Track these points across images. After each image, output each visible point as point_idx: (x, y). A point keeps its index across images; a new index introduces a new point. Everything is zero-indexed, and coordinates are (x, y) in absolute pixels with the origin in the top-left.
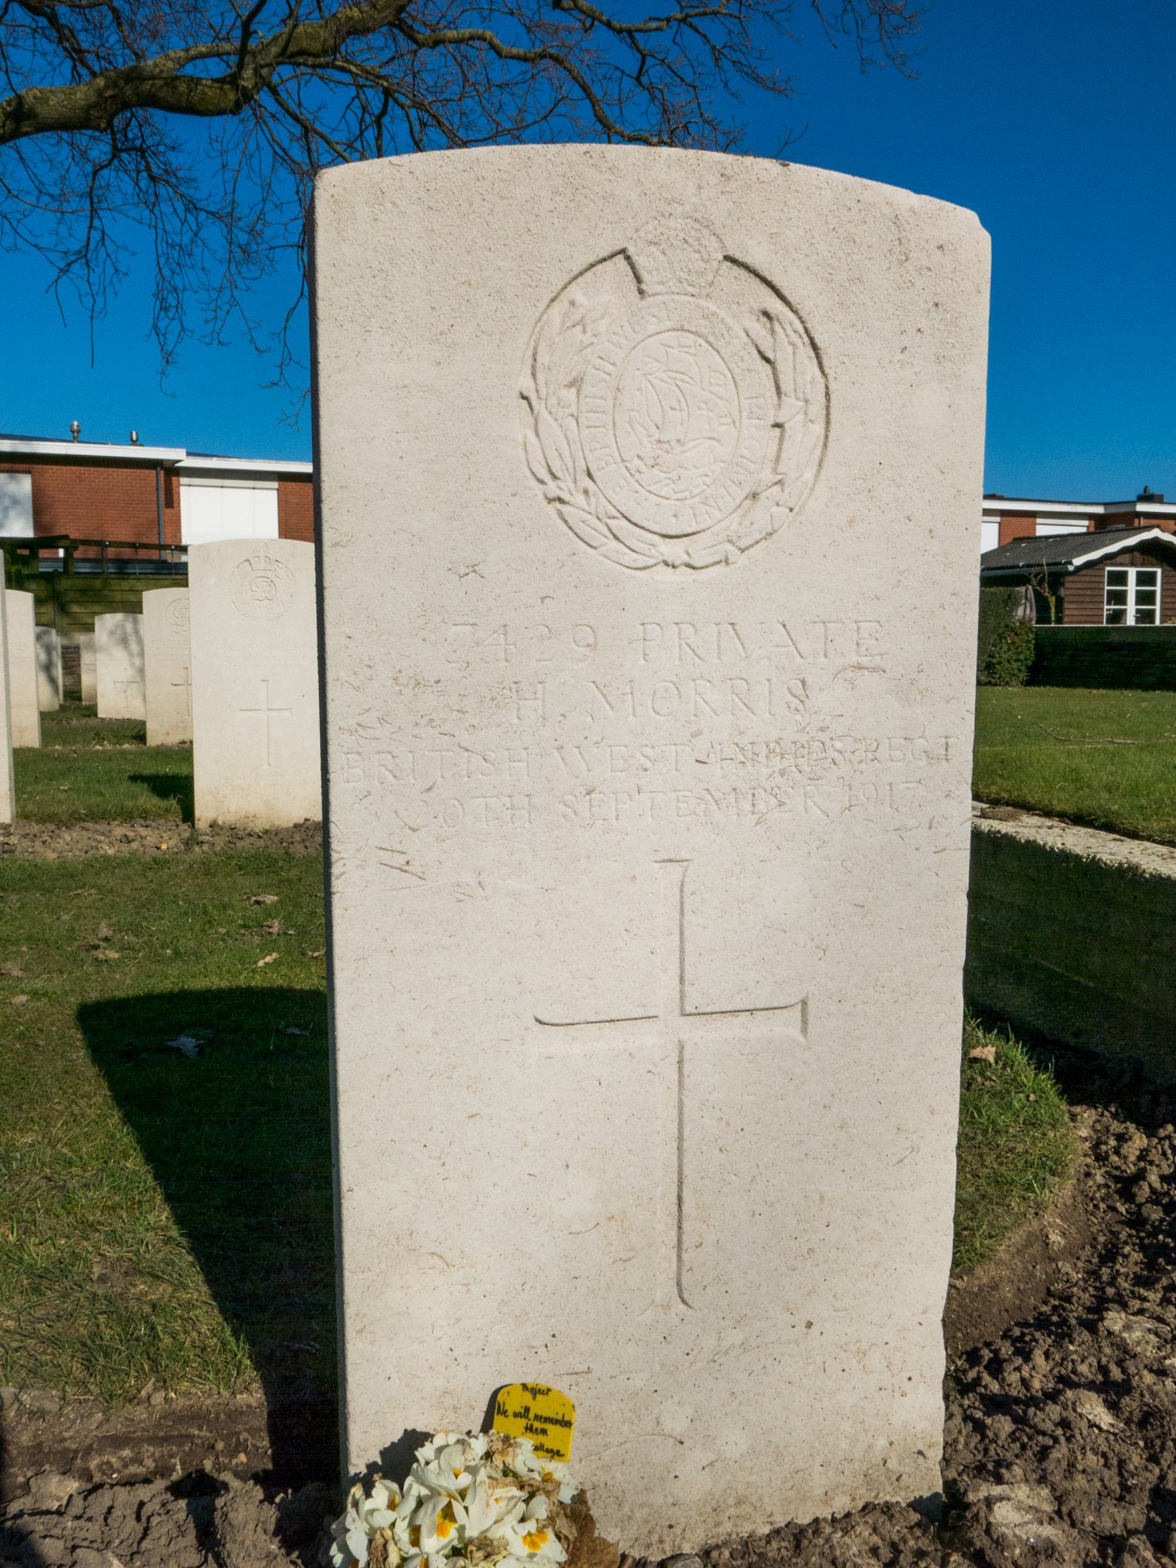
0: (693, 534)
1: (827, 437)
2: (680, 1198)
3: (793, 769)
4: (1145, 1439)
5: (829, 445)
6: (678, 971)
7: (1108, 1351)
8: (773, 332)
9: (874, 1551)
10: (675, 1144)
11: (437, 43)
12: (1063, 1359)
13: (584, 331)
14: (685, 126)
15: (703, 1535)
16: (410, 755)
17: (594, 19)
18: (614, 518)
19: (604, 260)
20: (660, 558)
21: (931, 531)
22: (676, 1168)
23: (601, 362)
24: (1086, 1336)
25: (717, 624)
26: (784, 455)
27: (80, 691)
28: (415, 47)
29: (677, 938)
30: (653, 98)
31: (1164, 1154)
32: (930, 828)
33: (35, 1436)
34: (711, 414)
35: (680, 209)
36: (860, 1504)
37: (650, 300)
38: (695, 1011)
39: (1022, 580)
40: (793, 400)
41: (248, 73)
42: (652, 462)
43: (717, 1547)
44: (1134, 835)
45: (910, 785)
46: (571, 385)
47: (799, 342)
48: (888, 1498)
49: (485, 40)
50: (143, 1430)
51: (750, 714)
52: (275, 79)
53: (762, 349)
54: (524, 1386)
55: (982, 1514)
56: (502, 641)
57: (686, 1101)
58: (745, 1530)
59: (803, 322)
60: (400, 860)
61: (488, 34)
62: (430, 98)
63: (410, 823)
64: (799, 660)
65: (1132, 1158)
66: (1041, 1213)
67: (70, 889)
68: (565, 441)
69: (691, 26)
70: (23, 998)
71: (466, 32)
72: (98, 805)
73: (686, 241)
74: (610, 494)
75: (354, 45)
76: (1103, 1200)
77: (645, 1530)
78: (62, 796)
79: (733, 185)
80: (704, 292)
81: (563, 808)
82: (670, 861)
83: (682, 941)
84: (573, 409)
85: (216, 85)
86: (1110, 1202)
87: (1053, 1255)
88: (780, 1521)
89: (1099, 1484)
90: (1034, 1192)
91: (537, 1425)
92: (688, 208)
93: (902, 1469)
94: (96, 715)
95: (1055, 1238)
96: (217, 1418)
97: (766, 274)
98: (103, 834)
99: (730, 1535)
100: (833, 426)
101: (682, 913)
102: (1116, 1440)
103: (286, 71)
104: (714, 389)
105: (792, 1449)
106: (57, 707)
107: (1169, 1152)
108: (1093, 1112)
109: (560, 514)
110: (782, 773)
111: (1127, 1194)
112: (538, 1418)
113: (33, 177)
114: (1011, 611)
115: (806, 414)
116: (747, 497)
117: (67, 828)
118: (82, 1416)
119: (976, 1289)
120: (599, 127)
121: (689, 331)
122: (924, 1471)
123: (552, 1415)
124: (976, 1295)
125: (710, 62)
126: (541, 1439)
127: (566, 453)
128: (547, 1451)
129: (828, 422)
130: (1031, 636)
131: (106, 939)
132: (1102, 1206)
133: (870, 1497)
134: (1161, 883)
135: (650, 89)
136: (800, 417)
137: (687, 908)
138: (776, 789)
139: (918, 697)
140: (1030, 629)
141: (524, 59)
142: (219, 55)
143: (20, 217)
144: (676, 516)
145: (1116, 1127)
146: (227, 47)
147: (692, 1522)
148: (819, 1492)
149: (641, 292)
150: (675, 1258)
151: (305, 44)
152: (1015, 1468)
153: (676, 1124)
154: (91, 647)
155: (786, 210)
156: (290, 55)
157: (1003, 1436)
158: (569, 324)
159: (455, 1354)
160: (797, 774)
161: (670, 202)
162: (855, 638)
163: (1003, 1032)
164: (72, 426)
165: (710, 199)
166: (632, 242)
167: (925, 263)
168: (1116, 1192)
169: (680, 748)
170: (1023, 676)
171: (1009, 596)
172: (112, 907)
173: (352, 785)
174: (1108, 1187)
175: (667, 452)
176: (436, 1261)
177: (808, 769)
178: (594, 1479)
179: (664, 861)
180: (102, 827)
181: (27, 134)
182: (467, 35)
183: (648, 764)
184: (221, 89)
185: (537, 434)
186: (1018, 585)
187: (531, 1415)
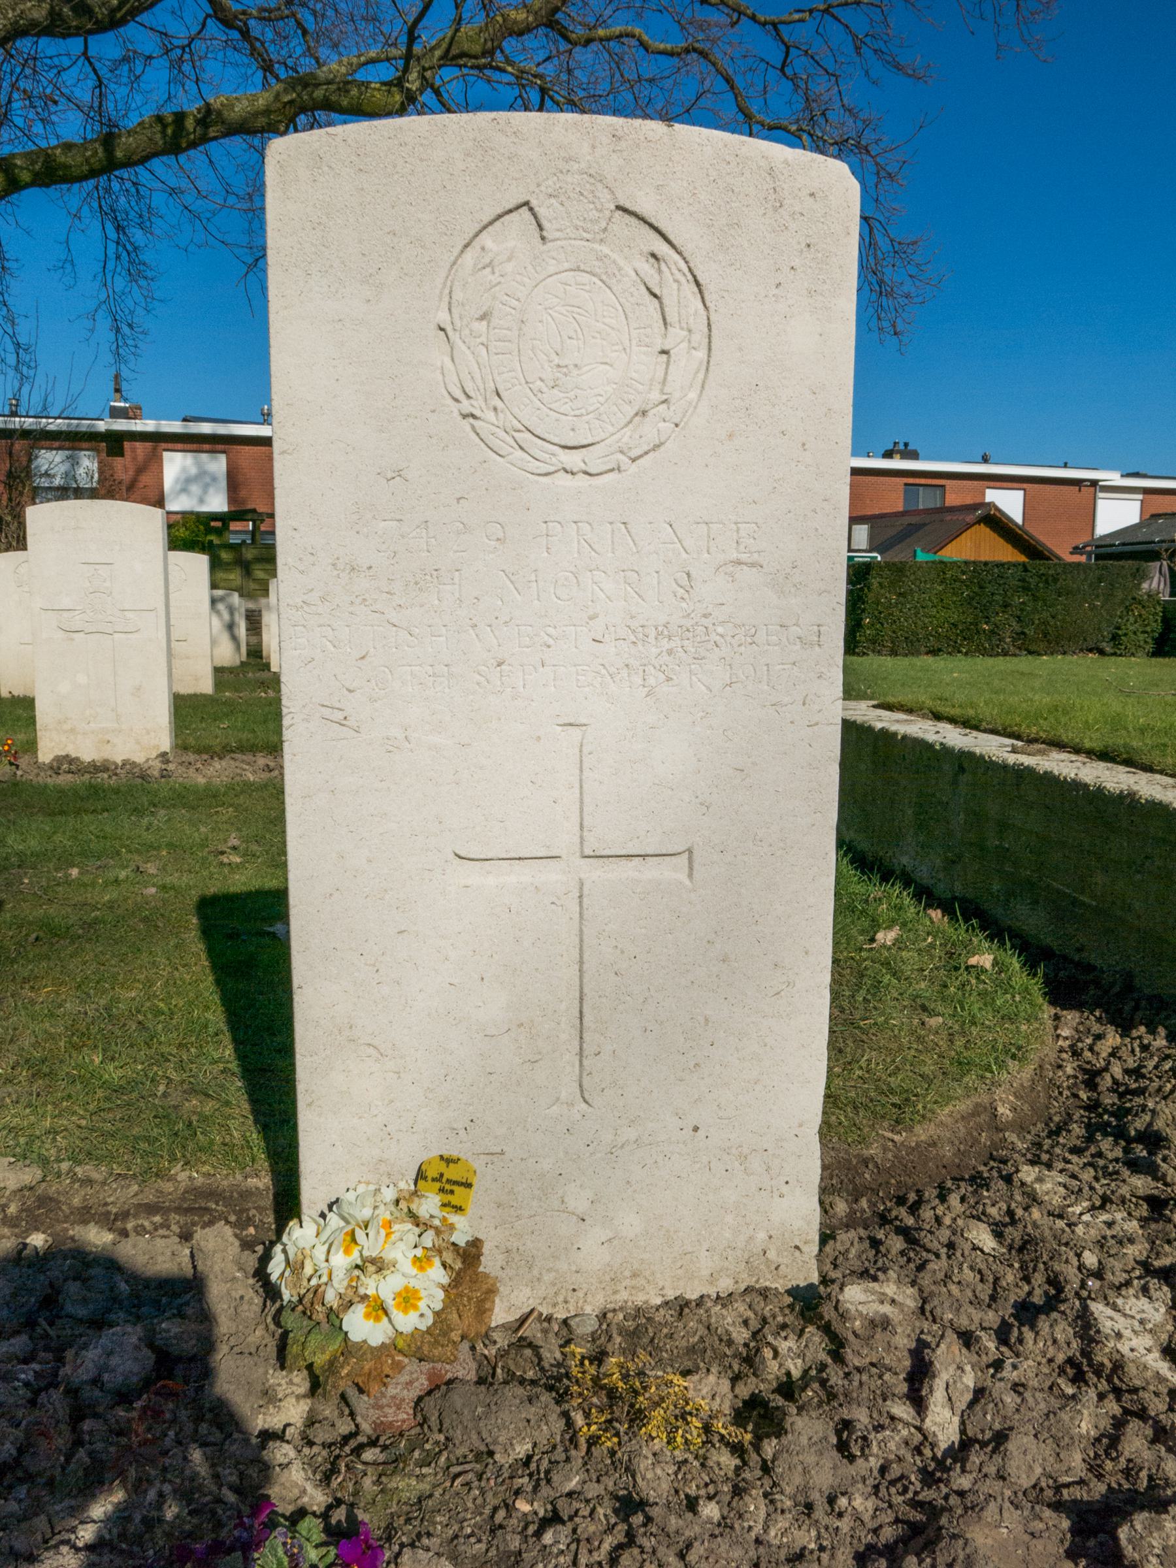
0: (589, 445)
1: (708, 362)
2: (581, 1012)
3: (680, 649)
4: (1022, 1262)
5: (711, 369)
6: (579, 820)
7: (1018, 1198)
8: (660, 271)
9: (746, 1323)
10: (577, 967)
11: (589, 41)
12: (977, 1203)
13: (493, 273)
14: (823, 114)
15: (602, 1300)
16: (347, 629)
17: (740, 13)
18: (519, 431)
19: (510, 211)
20: (560, 466)
21: (804, 445)
22: (578, 988)
23: (506, 298)
24: (1001, 1184)
25: (611, 523)
26: (669, 378)
27: (261, 651)
28: (570, 46)
29: (578, 791)
30: (797, 87)
31: (1133, 1051)
32: (804, 704)
33: (85, 1200)
34: (604, 343)
35: (576, 166)
36: (743, 1287)
37: (550, 245)
38: (592, 854)
39: (1154, 556)
40: (678, 330)
41: (413, 76)
42: (552, 384)
43: (614, 1310)
44: (1148, 769)
45: (785, 667)
46: (483, 317)
47: (683, 280)
48: (767, 1284)
49: (633, 36)
50: (171, 1201)
51: (640, 600)
52: (438, 82)
53: (650, 286)
54: (441, 1157)
55: (834, 1294)
56: (424, 534)
57: (584, 929)
58: (640, 1299)
59: (687, 262)
60: (339, 716)
61: (637, 31)
62: (581, 94)
63: (347, 685)
64: (684, 555)
65: (1104, 1055)
66: (993, 1089)
67: (210, 807)
68: (476, 366)
69: (833, 16)
70: (153, 890)
71: (617, 29)
72: (248, 740)
73: (582, 194)
74: (515, 410)
75: (510, 45)
76: (1069, 1088)
77: (552, 1291)
78: (219, 732)
79: (623, 144)
80: (598, 237)
81: (478, 677)
82: (571, 725)
83: (581, 794)
84: (483, 339)
85: (384, 88)
86: (1075, 1091)
87: (1001, 1126)
88: (671, 1295)
89: (970, 1294)
90: (992, 1072)
91: (448, 1187)
92: (583, 165)
93: (780, 1260)
94: (269, 670)
95: (1003, 1110)
96: (231, 1197)
97: (653, 221)
98: (249, 764)
99: (626, 1302)
100: (713, 352)
101: (581, 771)
102: (995, 1261)
103: (448, 73)
104: (607, 320)
105: (681, 1234)
106: (238, 663)
107: (1138, 1049)
108: (1078, 1015)
109: (473, 427)
110: (670, 652)
111: (1091, 1084)
112: (448, 1181)
113: (221, 179)
114: (1140, 584)
115: (689, 342)
116: (636, 414)
117: (221, 759)
118: (123, 1187)
119: (913, 1144)
120: (741, 117)
121: (584, 271)
122: (801, 1264)
123: (459, 1179)
124: (913, 1149)
125: (849, 49)
126: (450, 1198)
127: (477, 376)
128: (453, 1207)
129: (710, 349)
130: (1159, 609)
131: (234, 848)
132: (1066, 1093)
133: (751, 1282)
134: (1157, 809)
135: (793, 79)
136: (684, 345)
137: (585, 765)
138: (664, 667)
139: (793, 590)
140: (1158, 602)
141: (671, 54)
142: (388, 59)
143: (209, 215)
144: (573, 430)
145: (1096, 1028)
146: (394, 52)
147: (593, 1288)
148: (705, 1273)
149: (543, 238)
150: (577, 1063)
151: (466, 47)
152: (891, 1272)
153: (577, 950)
154: (268, 607)
155: (670, 164)
156: (450, 58)
157: (894, 1251)
158: (480, 266)
159: (388, 1129)
160: (682, 654)
161: (567, 160)
162: (735, 537)
163: (1002, 943)
164: (262, 410)
165: (602, 157)
166: (534, 196)
167: (797, 209)
168: (1083, 1082)
169: (579, 629)
170: (1150, 647)
171: (1138, 570)
172: (245, 822)
173: (299, 651)
174: (1077, 1077)
175: (566, 375)
176: (371, 1050)
177: (693, 650)
178: (509, 1244)
179: (565, 725)
180: (248, 757)
181: (215, 138)
182: (617, 33)
183: (551, 642)
184: (389, 91)
185: (453, 360)
186: (1153, 561)
187: (444, 1180)
